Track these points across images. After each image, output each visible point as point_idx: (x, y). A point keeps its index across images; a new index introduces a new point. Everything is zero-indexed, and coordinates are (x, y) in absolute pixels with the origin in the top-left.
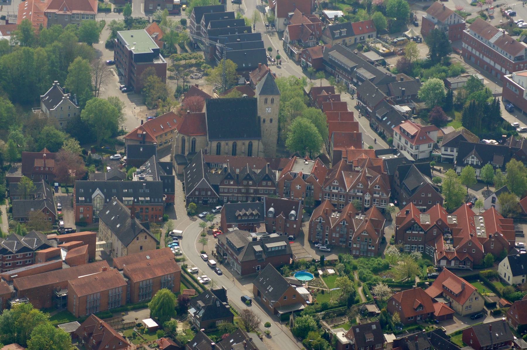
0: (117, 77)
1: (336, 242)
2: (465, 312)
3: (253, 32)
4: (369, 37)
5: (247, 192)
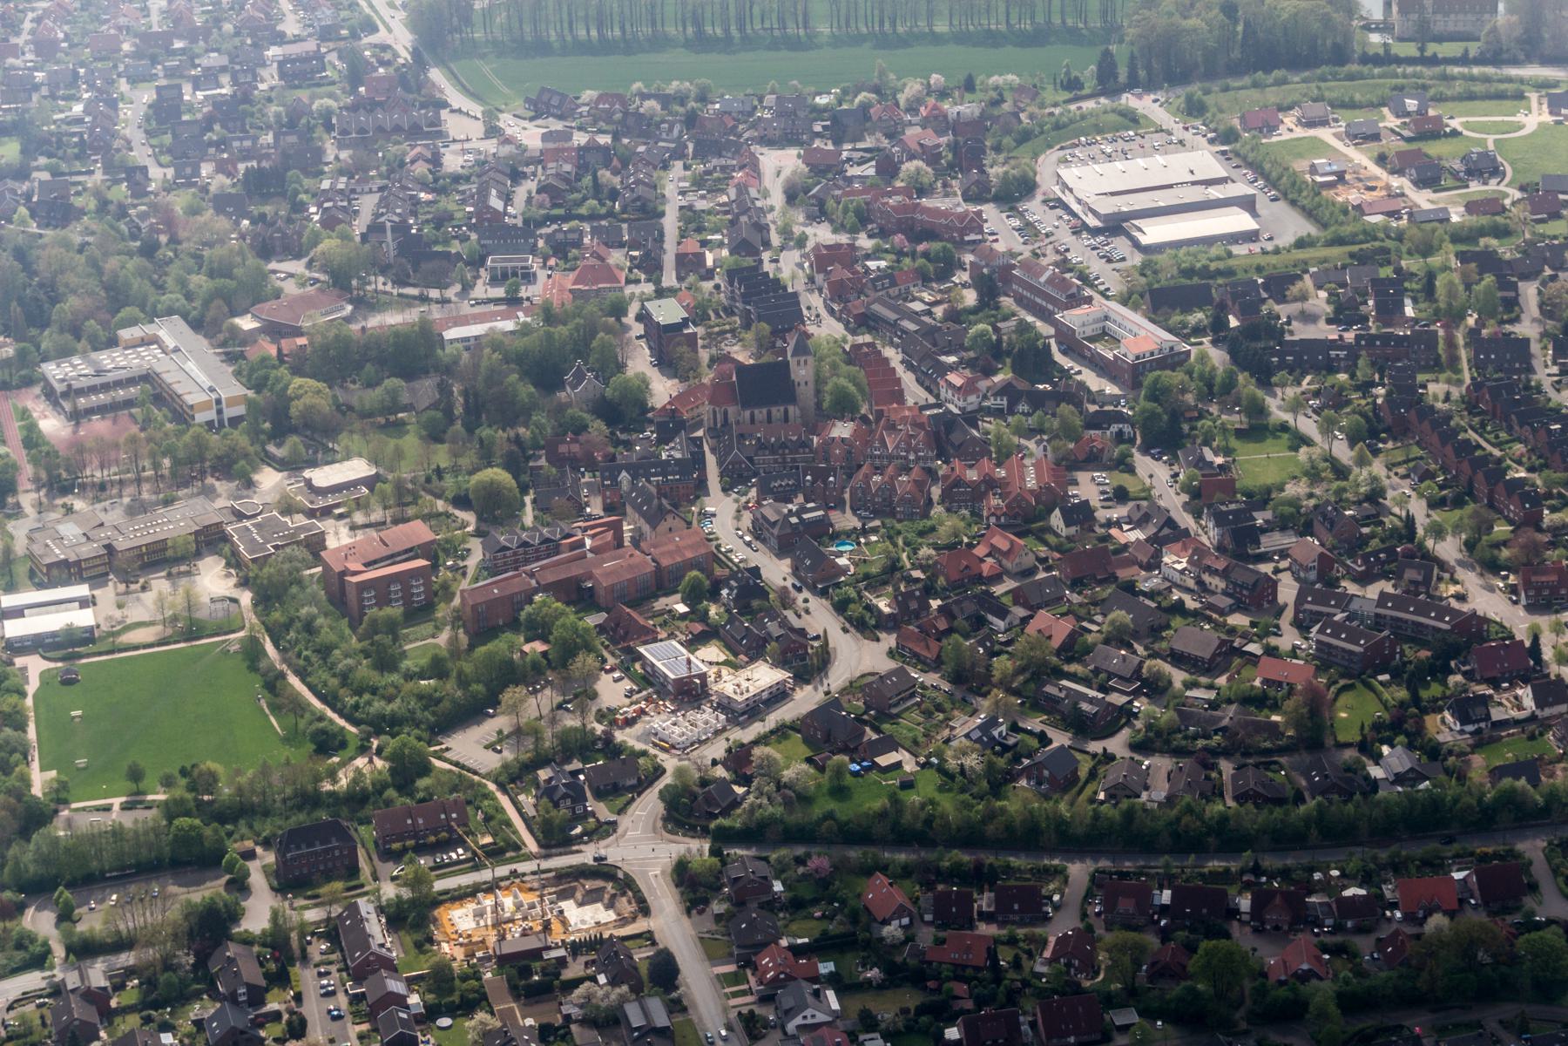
0: (647, 351)
1: (880, 507)
3: (790, 290)
5: (784, 461)
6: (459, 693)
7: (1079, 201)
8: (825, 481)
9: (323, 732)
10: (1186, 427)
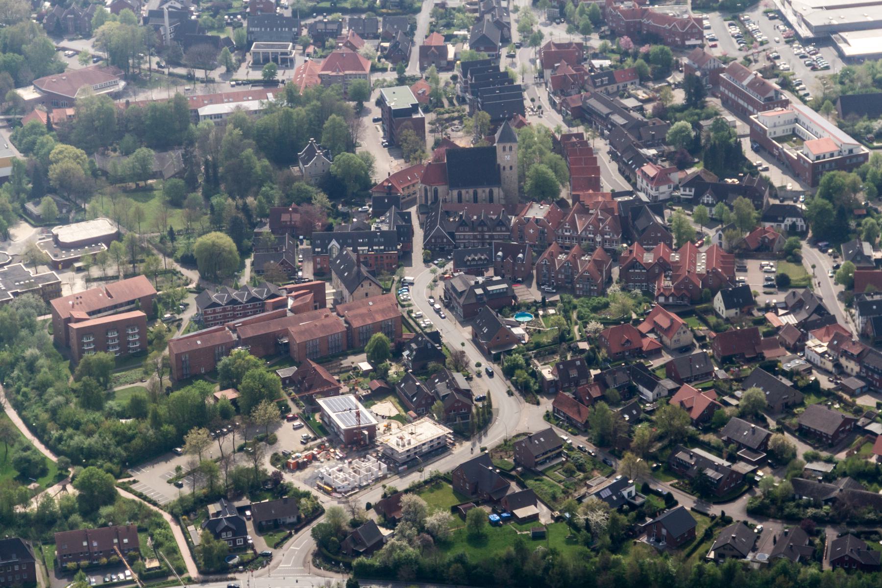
0: (381, 133)
1: (562, 283)
2: (673, 346)
4: (632, 84)
5: (483, 238)
6: (151, 432)
7: (795, 13)
8: (515, 257)
9: (27, 460)
10: (853, 224)
